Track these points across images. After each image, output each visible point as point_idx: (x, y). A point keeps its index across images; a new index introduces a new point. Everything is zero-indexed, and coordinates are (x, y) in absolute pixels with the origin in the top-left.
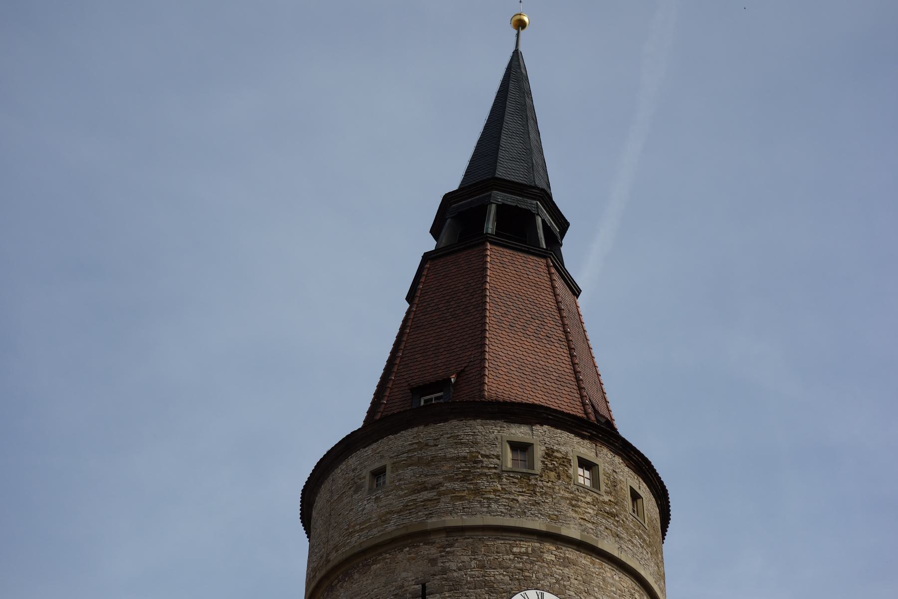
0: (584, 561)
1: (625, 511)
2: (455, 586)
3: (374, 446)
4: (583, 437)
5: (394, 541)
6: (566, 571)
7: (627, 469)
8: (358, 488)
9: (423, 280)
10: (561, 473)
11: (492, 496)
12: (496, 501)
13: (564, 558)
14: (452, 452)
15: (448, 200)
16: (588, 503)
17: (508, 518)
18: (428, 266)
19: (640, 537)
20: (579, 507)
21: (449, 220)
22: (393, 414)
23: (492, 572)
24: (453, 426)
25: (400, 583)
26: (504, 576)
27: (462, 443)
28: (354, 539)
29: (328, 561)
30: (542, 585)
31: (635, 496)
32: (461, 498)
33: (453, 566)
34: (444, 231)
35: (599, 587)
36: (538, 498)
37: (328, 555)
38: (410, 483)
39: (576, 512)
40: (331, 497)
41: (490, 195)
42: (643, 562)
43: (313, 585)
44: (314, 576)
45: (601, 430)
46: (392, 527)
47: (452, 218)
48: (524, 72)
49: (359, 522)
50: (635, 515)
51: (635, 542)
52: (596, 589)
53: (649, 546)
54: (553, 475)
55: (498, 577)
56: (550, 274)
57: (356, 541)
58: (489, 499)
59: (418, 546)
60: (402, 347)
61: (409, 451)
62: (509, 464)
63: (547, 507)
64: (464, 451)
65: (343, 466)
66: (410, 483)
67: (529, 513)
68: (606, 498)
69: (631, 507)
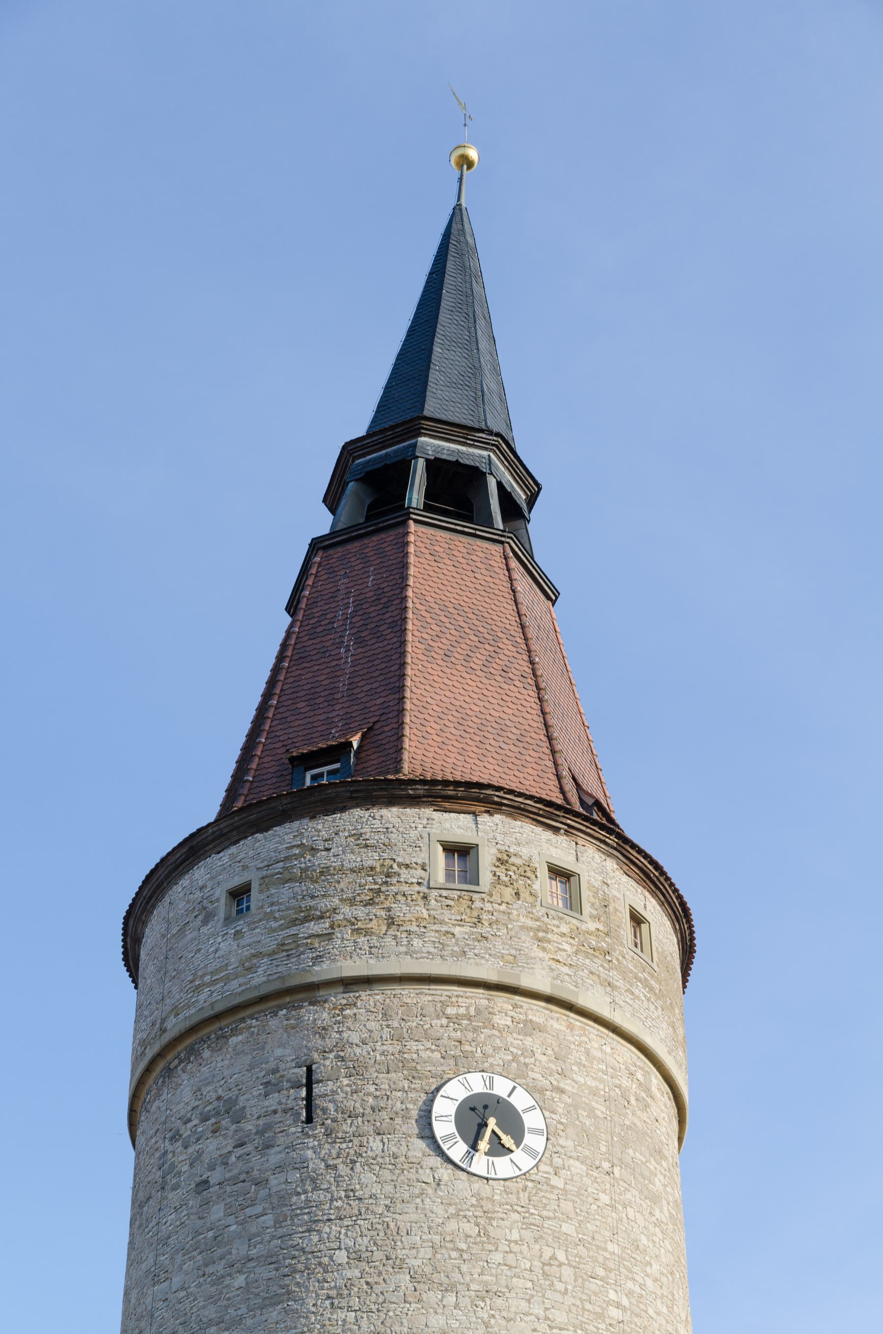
0: (556, 1026)
1: (622, 944)
2: (356, 1070)
3: (233, 850)
4: (556, 830)
5: (263, 999)
6: (528, 1041)
7: (625, 878)
8: (209, 917)
9: (310, 582)
10: (522, 890)
11: (414, 928)
12: (421, 936)
13: (525, 1022)
14: (352, 859)
15: (350, 450)
16: (563, 935)
17: (438, 960)
18: (317, 559)
19: (646, 984)
20: (549, 941)
21: (351, 484)
22: (261, 803)
23: (413, 1045)
24: (356, 817)
25: (272, 1065)
26: (433, 1051)
27: (366, 846)
28: (202, 997)
29: (163, 1031)
30: (492, 1065)
31: (637, 920)
32: (368, 932)
33: (355, 1038)
34: (343, 502)
35: (580, 1064)
36: (485, 929)
37: (163, 1020)
38: (288, 909)
39: (544, 949)
40: (168, 929)
41: (414, 446)
42: (649, 1023)
43: (142, 1066)
44: (143, 1054)
45: (589, 817)
46: (260, 979)
47: (356, 480)
48: (469, 239)
49: (210, 969)
50: (638, 951)
51: (637, 992)
52: (575, 1068)
53: (658, 997)
54: (508, 892)
55: (423, 1054)
56: (508, 570)
57: (207, 1000)
58: (409, 932)
59: (301, 1007)
60: (278, 691)
61: (287, 858)
62: (440, 877)
63: (498, 944)
64: (371, 859)
65: (185, 881)
66: (288, 909)
67: (470, 954)
68: (592, 926)
69: (631, 937)
